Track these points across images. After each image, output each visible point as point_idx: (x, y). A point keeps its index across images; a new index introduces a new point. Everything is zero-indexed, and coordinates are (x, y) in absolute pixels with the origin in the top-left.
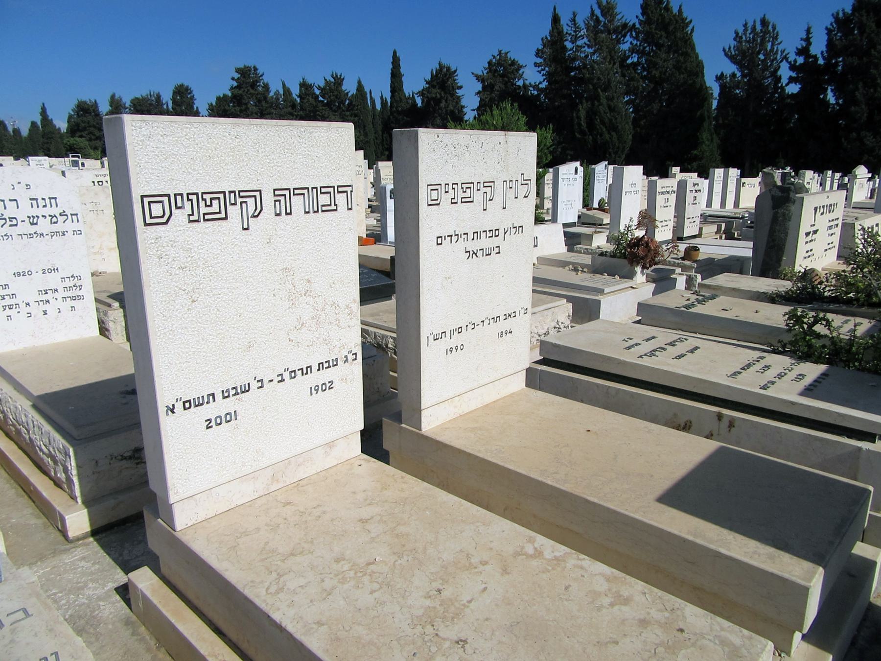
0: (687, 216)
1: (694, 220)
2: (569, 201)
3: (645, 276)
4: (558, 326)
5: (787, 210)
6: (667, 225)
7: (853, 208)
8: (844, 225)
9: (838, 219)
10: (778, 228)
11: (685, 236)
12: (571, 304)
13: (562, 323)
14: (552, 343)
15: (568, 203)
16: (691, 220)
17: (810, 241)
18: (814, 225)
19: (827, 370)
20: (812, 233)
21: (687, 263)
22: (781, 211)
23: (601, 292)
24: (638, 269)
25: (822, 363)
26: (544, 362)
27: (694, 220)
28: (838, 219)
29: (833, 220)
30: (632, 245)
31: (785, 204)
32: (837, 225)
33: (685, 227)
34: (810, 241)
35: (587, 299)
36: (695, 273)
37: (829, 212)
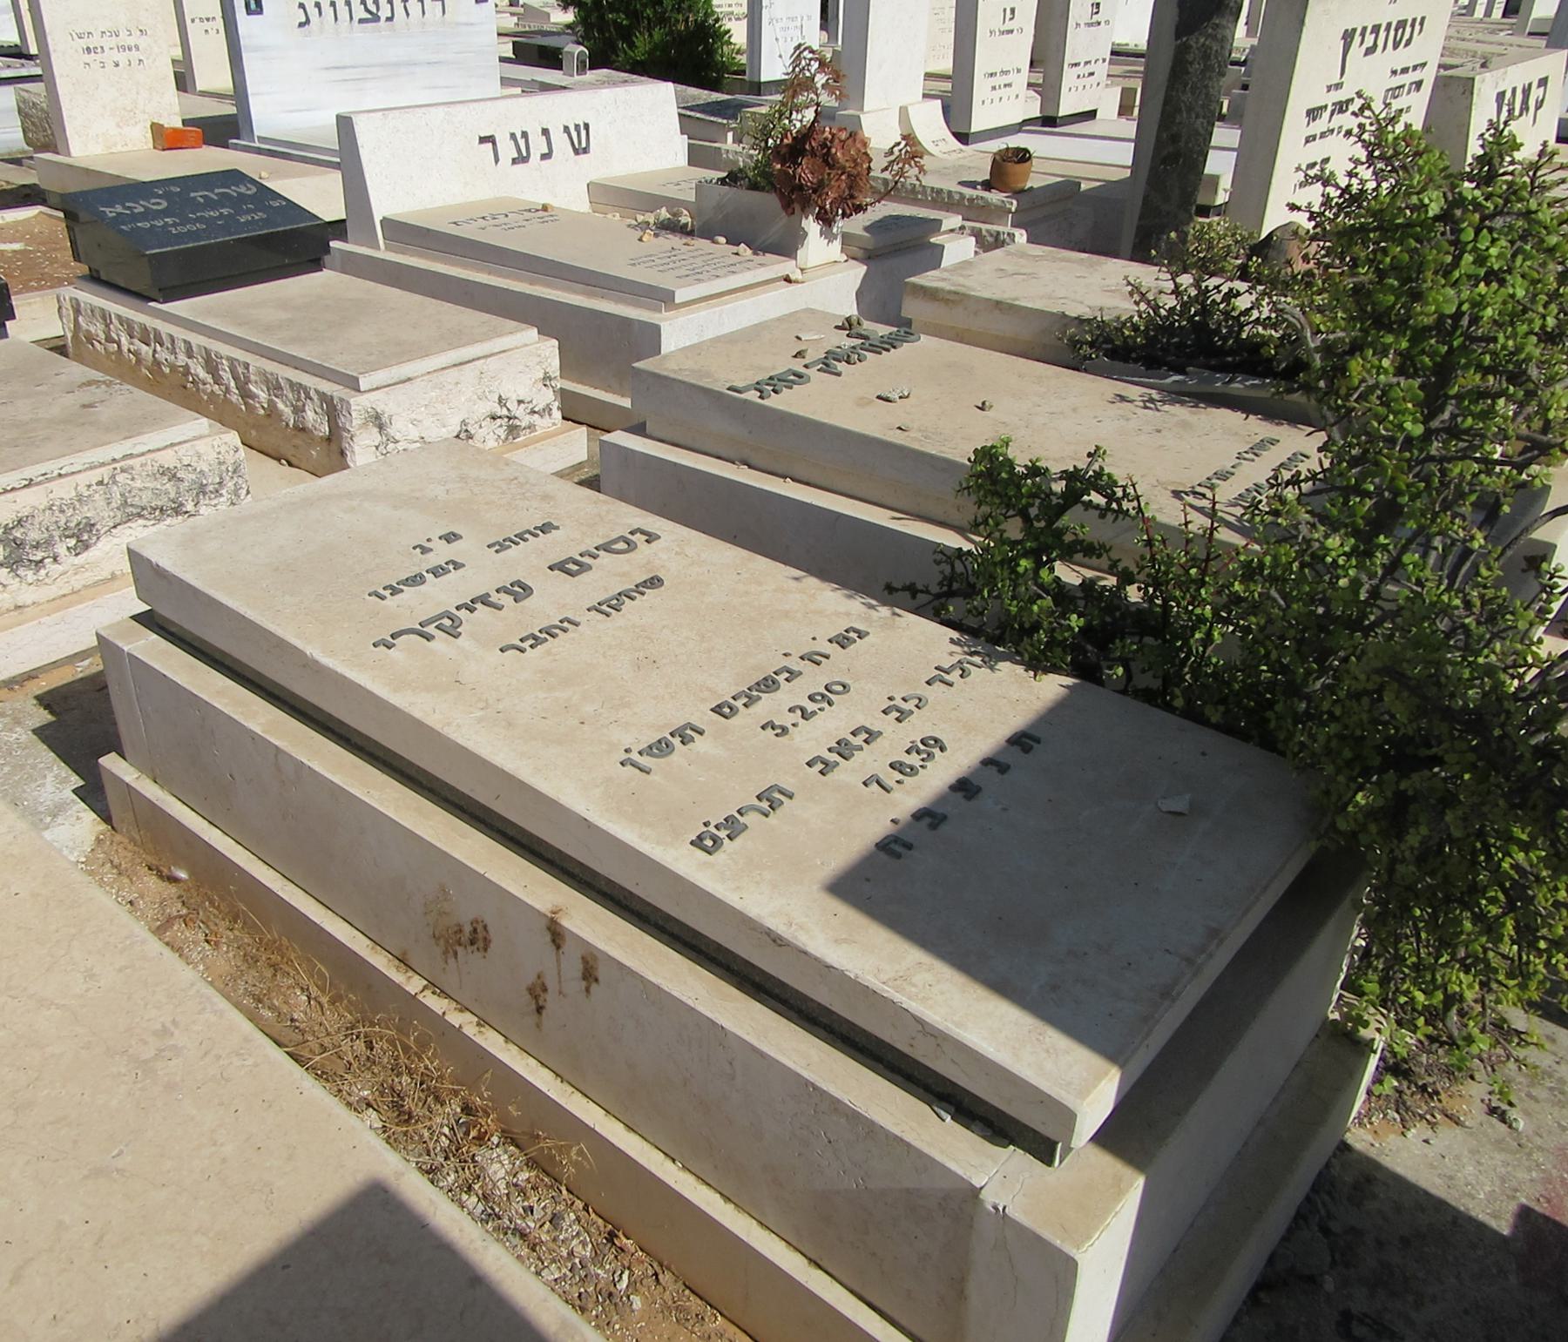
0: (1068, 59)
1: (1089, 69)
2: (793, 19)
3: (837, 244)
4: (505, 412)
5: (1214, 37)
6: (1009, 85)
7: (1530, 34)
8: (1441, 84)
9: (1424, 65)
10: (1187, 97)
11: (1060, 114)
12: (556, 343)
13: (520, 402)
14: (149, 561)
15: (792, 25)
16: (1081, 70)
17: (1323, 135)
18: (1338, 86)
19: (1055, 714)
20: (1330, 109)
21: (995, 197)
22: (1197, 41)
23: (664, 299)
24: (811, 226)
25: (1055, 669)
26: (147, 620)
27: (1089, 69)
28: (1424, 65)
29: (1405, 71)
30: (784, 151)
31: (1209, 20)
32: (1419, 84)
33: (1064, 90)
34: (1323, 135)
35: (626, 322)
36: (1012, 226)
37: (1396, 46)
